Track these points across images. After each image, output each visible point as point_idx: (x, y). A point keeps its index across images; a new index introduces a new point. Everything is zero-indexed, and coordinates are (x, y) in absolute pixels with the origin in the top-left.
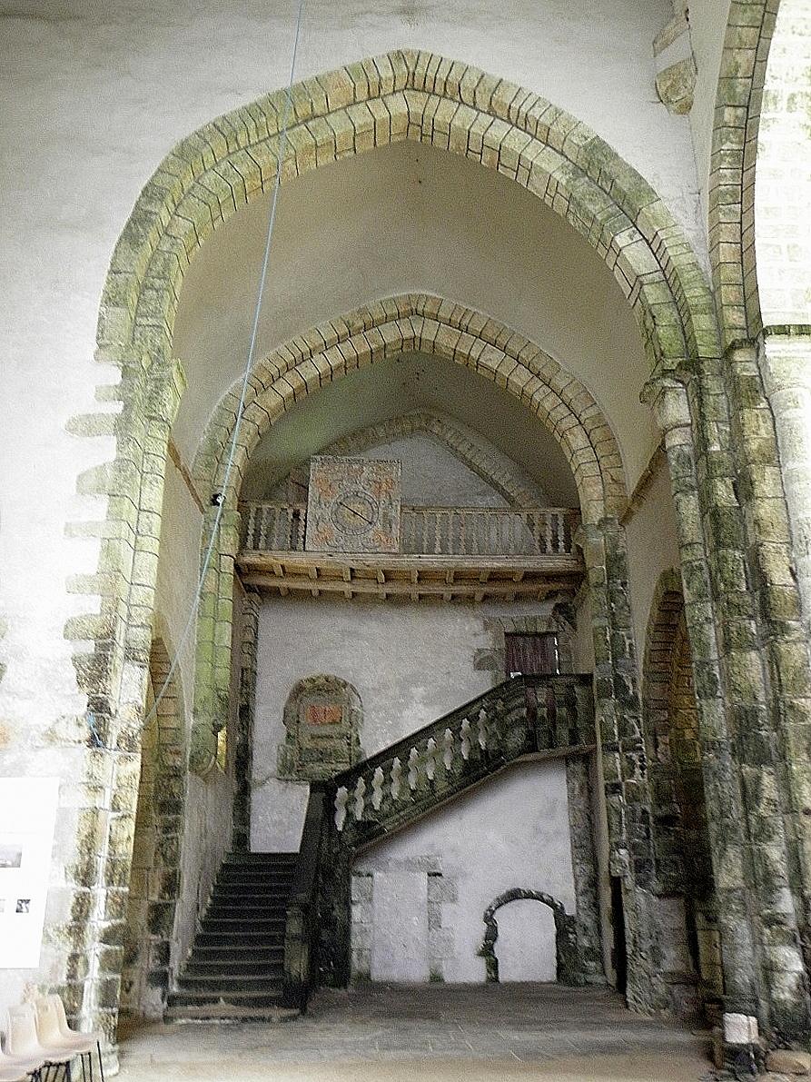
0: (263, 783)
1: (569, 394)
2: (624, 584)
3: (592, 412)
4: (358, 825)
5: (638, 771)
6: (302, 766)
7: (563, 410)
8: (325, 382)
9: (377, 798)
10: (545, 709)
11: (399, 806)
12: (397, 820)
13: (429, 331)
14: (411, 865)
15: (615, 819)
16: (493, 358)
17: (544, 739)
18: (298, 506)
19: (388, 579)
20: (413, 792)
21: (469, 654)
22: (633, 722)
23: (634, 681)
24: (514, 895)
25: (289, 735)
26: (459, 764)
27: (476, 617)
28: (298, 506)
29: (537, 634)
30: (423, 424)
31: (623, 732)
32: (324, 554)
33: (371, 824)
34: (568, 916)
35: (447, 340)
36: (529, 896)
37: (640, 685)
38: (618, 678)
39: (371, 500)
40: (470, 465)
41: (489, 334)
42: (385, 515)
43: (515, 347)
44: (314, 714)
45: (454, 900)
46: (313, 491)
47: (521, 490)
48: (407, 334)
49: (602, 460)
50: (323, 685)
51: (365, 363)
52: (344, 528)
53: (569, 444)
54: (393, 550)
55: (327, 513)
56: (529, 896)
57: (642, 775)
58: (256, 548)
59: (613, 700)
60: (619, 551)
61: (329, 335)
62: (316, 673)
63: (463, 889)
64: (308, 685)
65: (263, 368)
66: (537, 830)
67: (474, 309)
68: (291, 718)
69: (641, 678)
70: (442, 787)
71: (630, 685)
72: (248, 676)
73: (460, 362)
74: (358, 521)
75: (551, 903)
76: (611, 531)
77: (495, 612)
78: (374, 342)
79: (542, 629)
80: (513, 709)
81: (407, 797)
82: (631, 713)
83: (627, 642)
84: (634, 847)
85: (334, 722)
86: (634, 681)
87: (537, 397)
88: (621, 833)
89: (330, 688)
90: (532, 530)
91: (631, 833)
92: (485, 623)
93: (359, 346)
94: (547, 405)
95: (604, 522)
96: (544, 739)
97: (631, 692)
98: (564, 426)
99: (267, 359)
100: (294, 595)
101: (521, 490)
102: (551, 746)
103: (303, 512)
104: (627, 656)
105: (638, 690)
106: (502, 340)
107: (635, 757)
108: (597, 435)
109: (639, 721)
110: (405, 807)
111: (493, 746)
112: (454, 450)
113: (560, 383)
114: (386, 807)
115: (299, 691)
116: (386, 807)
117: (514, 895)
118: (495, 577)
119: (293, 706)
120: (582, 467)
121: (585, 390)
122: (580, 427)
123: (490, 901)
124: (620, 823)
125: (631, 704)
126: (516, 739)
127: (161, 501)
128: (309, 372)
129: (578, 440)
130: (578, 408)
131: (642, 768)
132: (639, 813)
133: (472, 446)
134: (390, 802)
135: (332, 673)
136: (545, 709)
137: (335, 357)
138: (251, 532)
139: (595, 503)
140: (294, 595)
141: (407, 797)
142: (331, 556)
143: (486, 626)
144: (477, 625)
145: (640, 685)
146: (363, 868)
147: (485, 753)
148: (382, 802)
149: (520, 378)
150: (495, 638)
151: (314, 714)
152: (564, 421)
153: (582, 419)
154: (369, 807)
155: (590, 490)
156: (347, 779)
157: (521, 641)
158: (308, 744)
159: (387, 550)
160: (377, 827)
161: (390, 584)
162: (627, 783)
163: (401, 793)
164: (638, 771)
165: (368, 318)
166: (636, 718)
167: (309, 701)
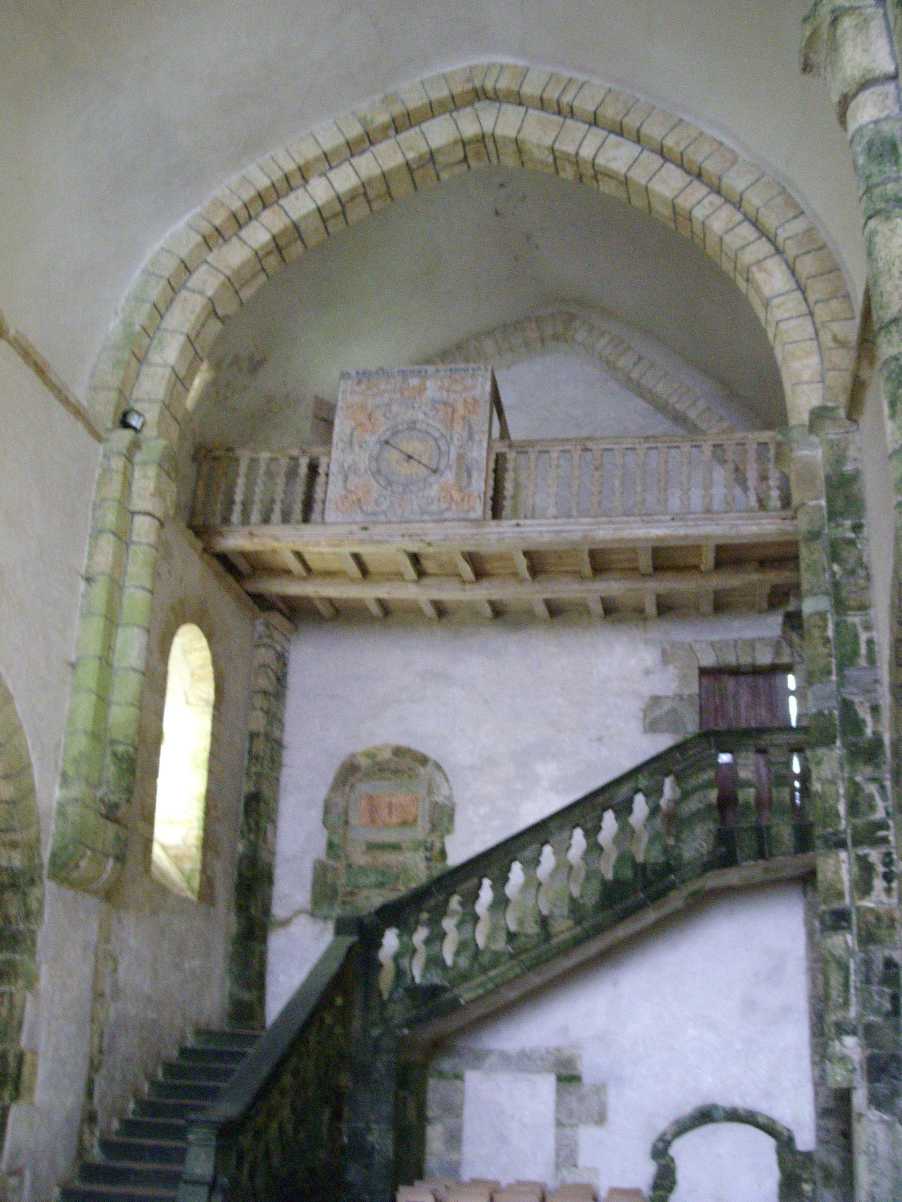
0: (285, 923)
1: (754, 200)
2: (857, 528)
3: (797, 226)
4: (414, 991)
5: (879, 884)
6: (352, 894)
7: (746, 231)
8: (337, 226)
9: (448, 952)
10: (752, 791)
11: (485, 959)
12: (482, 984)
13: (505, 122)
14: (523, 1062)
15: (836, 979)
16: (619, 156)
17: (747, 843)
18: (316, 450)
19: (480, 574)
20: (511, 936)
21: (635, 706)
22: (872, 788)
23: (875, 709)
24: (705, 1116)
25: (331, 845)
26: (595, 887)
27: (647, 642)
28: (316, 450)
29: (756, 671)
30: (560, 329)
31: (854, 808)
32: (355, 528)
33: (434, 991)
34: (801, 1153)
35: (538, 132)
36: (734, 1116)
37: (886, 714)
38: (847, 706)
39: (437, 434)
40: (640, 390)
41: (610, 112)
42: (461, 457)
43: (654, 130)
44: (373, 810)
45: (601, 1119)
46: (342, 426)
47: (725, 425)
48: (469, 130)
49: (818, 310)
50: (388, 762)
51: (401, 187)
52: (390, 483)
53: (758, 291)
54: (472, 515)
55: (362, 458)
56: (734, 1116)
57: (888, 891)
58: (245, 521)
59: (838, 750)
60: (849, 468)
61: (331, 140)
62: (378, 742)
63: (618, 1103)
64: (364, 762)
65: (219, 203)
66: (749, 1006)
67: (581, 77)
68: (335, 817)
69: (886, 699)
70: (563, 927)
71: (869, 720)
72: (260, 746)
73: (568, 174)
74: (414, 469)
75: (769, 1128)
76: (832, 432)
77: (683, 633)
78: (411, 148)
79: (765, 658)
80: (694, 790)
81: (500, 944)
82: (869, 770)
83: (864, 636)
84: (869, 1033)
85: (404, 824)
86: (875, 709)
87: (698, 214)
88: (846, 1004)
89: (405, 764)
90: (745, 489)
91: (865, 1004)
92: (664, 653)
93: (388, 156)
94: (717, 226)
95: (819, 415)
96: (747, 843)
97: (869, 731)
98: (747, 257)
99: (230, 189)
100: (343, 615)
101: (725, 425)
102: (761, 854)
103: (323, 461)
104: (863, 662)
105: (881, 727)
106: (632, 122)
107: (875, 855)
108: (807, 266)
109: (883, 788)
110: (494, 964)
111: (656, 856)
112: (610, 366)
113: (736, 182)
114: (464, 962)
115: (349, 773)
116: (464, 962)
117: (705, 1116)
118: (666, 560)
119: (339, 800)
120: (782, 326)
121: (783, 191)
122: (777, 260)
123: (663, 1124)
124: (846, 985)
125: (866, 753)
126: (697, 843)
127: (175, 490)
128: (299, 205)
129: (773, 280)
130: (770, 221)
131: (888, 877)
132: (878, 967)
133: (640, 358)
134: (469, 953)
135: (404, 742)
136: (752, 791)
137: (344, 179)
138: (238, 497)
139: (805, 387)
140: (343, 615)
141: (500, 944)
142: (365, 529)
143: (666, 658)
144: (649, 656)
145: (886, 714)
146: (446, 1065)
147: (640, 869)
148: (457, 953)
149: (668, 184)
150: (683, 678)
151: (373, 810)
152: (748, 250)
153: (780, 240)
154: (435, 961)
155: (796, 365)
156: (397, 914)
157: (730, 684)
158: (360, 859)
159: (462, 516)
160: (448, 995)
161: (485, 583)
162: (858, 908)
163: (491, 937)
164: (879, 884)
165: (398, 109)
166: (874, 780)
167: (364, 788)
